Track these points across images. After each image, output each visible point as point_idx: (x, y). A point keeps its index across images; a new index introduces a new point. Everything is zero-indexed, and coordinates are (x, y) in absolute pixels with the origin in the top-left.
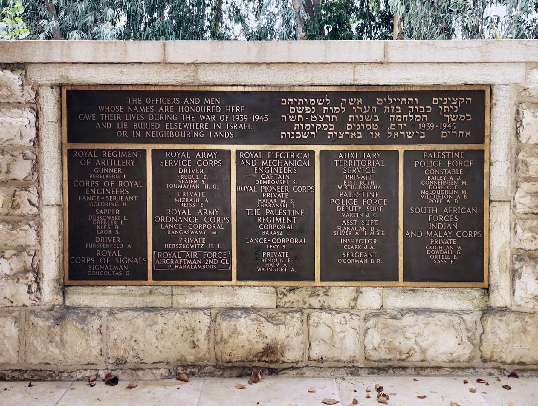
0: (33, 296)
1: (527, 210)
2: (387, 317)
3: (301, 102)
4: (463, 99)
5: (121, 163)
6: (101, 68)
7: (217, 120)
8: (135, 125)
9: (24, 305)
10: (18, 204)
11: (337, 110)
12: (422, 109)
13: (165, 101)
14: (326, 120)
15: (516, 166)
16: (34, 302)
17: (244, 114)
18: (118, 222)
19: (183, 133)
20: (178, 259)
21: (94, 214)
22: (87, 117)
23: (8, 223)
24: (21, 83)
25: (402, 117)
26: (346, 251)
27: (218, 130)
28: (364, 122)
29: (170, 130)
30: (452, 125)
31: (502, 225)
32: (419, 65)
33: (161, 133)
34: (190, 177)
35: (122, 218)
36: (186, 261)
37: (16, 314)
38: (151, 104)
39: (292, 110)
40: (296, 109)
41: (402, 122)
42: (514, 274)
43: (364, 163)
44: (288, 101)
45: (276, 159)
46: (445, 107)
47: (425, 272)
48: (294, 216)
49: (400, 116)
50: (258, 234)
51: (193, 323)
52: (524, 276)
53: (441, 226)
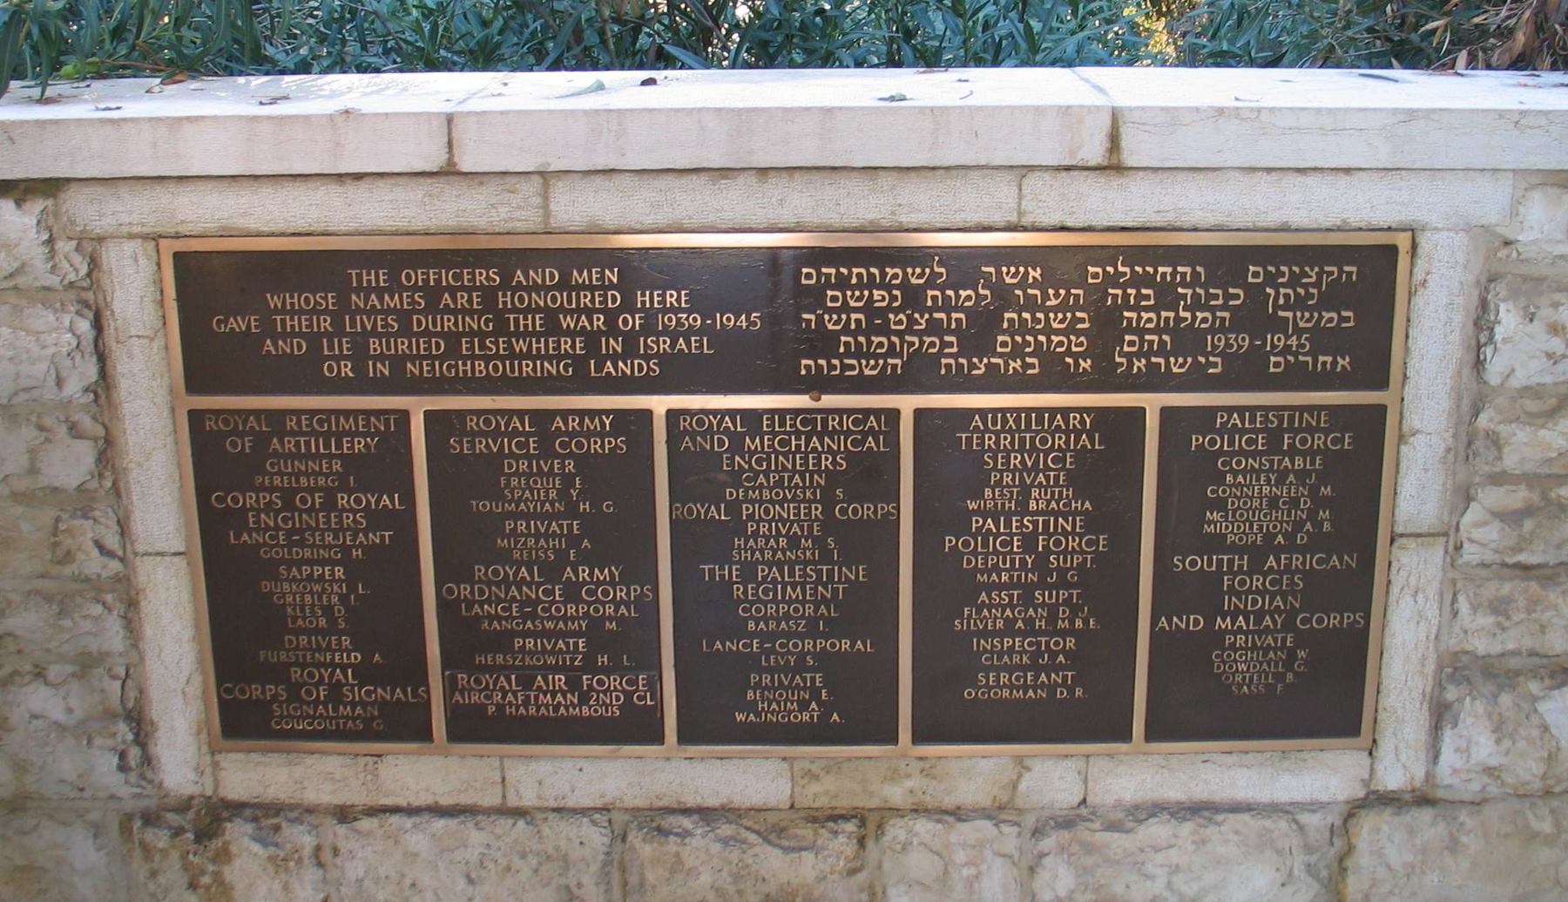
0: (133, 777)
1: (1489, 557)
2: (1097, 825)
3: (859, 275)
4: (1335, 269)
5: (339, 446)
6: (266, 191)
7: (612, 330)
8: (374, 344)
9: (112, 797)
10: (69, 552)
11: (969, 298)
12: (1216, 297)
13: (457, 277)
14: (934, 328)
15: (1469, 444)
16: (138, 790)
17: (689, 311)
18: (344, 599)
19: (512, 365)
20: (515, 694)
21: (276, 577)
22: (237, 324)
23: (48, 598)
24: (45, 237)
25: (1159, 317)
26: (987, 670)
27: (615, 358)
28: (1048, 331)
29: (474, 357)
30: (1299, 338)
31: (1420, 595)
32: (1210, 175)
33: (449, 367)
34: (535, 482)
35: (352, 588)
36: (537, 697)
37: (94, 816)
38: (415, 288)
39: (834, 299)
40: (844, 296)
41: (1157, 331)
42: (1440, 715)
43: (1044, 441)
44: (819, 274)
45: (785, 433)
46: (1282, 291)
47: (1200, 708)
48: (840, 582)
49: (1152, 315)
50: (739, 631)
51: (563, 843)
52: (1466, 720)
53: (1255, 602)
